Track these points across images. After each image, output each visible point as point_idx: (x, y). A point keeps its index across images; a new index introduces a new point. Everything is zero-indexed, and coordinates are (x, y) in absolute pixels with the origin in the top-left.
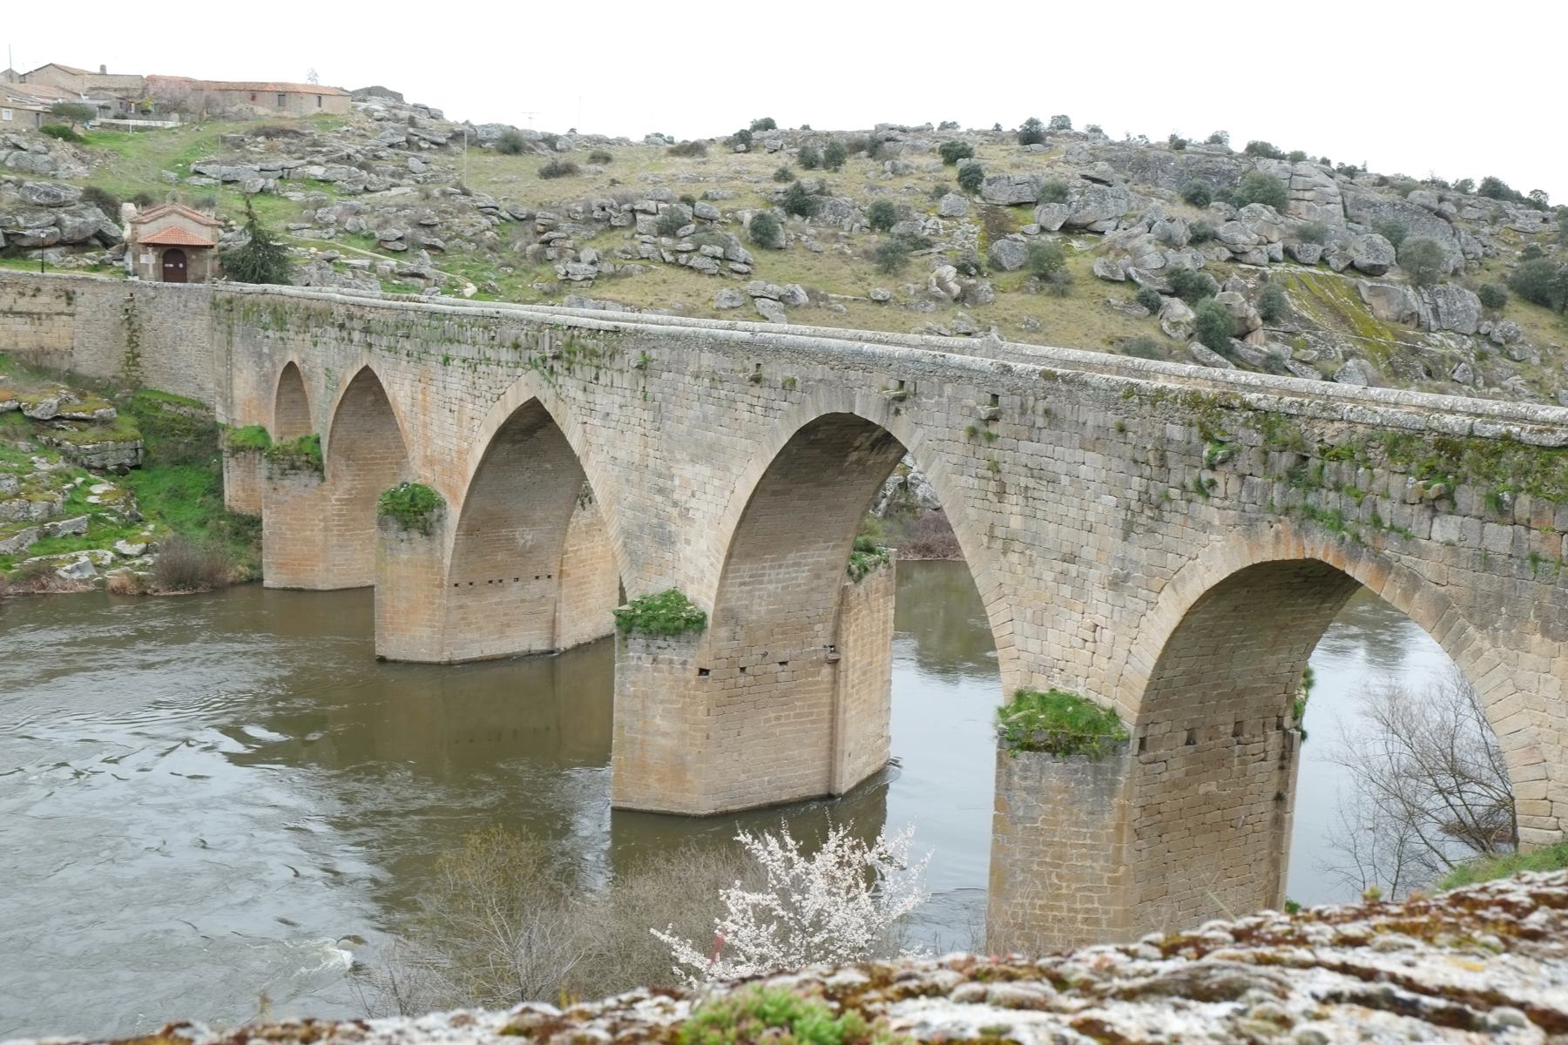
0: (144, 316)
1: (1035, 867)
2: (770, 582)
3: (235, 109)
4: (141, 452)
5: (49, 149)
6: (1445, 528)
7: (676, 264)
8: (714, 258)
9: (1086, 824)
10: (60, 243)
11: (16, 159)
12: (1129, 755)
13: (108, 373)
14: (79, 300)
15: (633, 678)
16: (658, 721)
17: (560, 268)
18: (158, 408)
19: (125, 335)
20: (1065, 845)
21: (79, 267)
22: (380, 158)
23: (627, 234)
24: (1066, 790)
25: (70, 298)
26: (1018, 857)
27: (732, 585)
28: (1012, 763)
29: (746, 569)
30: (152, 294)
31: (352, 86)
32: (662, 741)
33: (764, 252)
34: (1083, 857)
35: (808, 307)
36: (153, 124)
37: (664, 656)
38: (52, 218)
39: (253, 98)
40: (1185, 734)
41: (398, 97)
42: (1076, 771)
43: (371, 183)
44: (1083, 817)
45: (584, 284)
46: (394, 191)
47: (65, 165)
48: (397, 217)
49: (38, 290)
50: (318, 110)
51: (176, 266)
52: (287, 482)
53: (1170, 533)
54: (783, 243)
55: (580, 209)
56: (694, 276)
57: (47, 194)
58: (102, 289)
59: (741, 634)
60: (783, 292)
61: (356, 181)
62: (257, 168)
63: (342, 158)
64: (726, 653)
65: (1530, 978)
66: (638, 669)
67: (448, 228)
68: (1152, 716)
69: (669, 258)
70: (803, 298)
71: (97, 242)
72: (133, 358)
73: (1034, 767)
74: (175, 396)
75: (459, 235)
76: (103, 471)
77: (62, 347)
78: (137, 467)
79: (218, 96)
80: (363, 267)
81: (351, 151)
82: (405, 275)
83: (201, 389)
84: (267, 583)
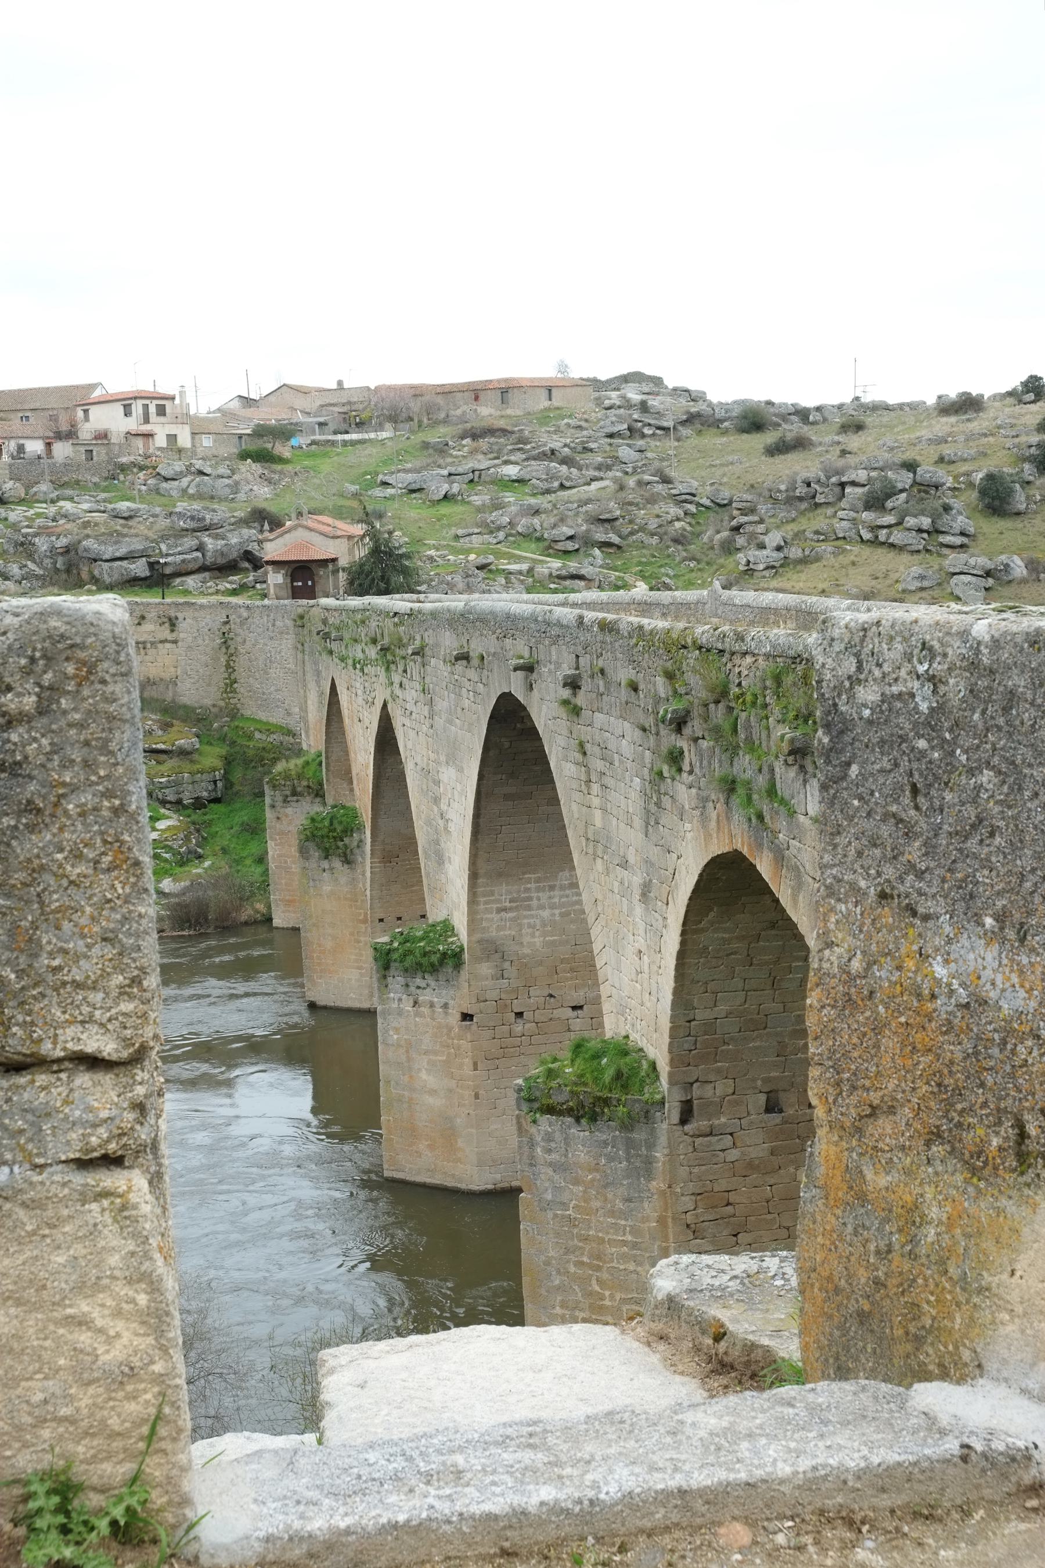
0: (239, 639)
1: (572, 1269)
2: (542, 907)
3: (459, 412)
4: (220, 784)
5: (233, 472)
7: (875, 542)
8: (920, 531)
9: (624, 1215)
10: (203, 569)
11: (198, 486)
12: (666, 1125)
13: (208, 702)
14: (182, 626)
15: (395, 1024)
16: (424, 1075)
17: (741, 558)
18: (250, 737)
19: (223, 660)
20: (602, 1241)
21: (217, 592)
22: (591, 450)
23: (830, 511)
24: (596, 1168)
25: (173, 624)
26: (552, 1253)
27: (488, 911)
28: (533, 1130)
29: (504, 892)
30: (245, 614)
31: (604, 375)
32: (430, 1100)
33: (995, 519)
34: (624, 1257)
35: (1023, 581)
36: (366, 436)
37: (425, 997)
38: (194, 543)
39: (477, 398)
40: (763, 1098)
41: (657, 381)
42: (605, 1143)
43: (568, 479)
44: (620, 1205)
45: (766, 573)
46: (595, 486)
47: (247, 488)
48: (577, 514)
49: (143, 618)
50: (547, 404)
51: (305, 584)
52: (289, 811)
54: (1022, 507)
55: (783, 487)
56: (892, 554)
57: (192, 518)
58: (202, 613)
59: (511, 971)
60: (990, 565)
61: (553, 478)
62: (445, 472)
63: (544, 454)
64: (493, 995)
65: (527, 1457)
66: (400, 1013)
67: (631, 522)
68: (695, 1073)
69: (867, 535)
70: (1019, 568)
71: (246, 565)
72: (230, 685)
73: (558, 1136)
74: (267, 723)
75: (642, 529)
76: (178, 805)
77: (167, 676)
78: (217, 800)
79: (440, 400)
80: (520, 573)
81: (556, 445)
82: (564, 578)
83: (289, 714)
84: (277, 922)
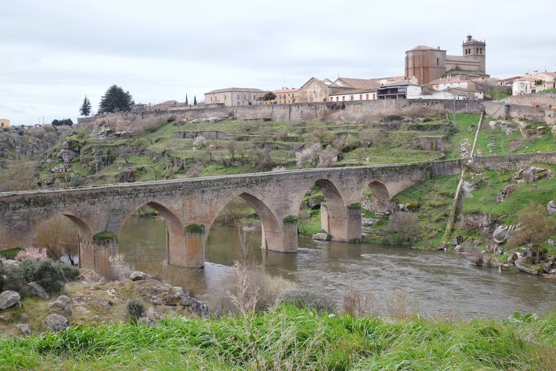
6: (383, 176)
18: (461, 79)
53: (363, 181)
